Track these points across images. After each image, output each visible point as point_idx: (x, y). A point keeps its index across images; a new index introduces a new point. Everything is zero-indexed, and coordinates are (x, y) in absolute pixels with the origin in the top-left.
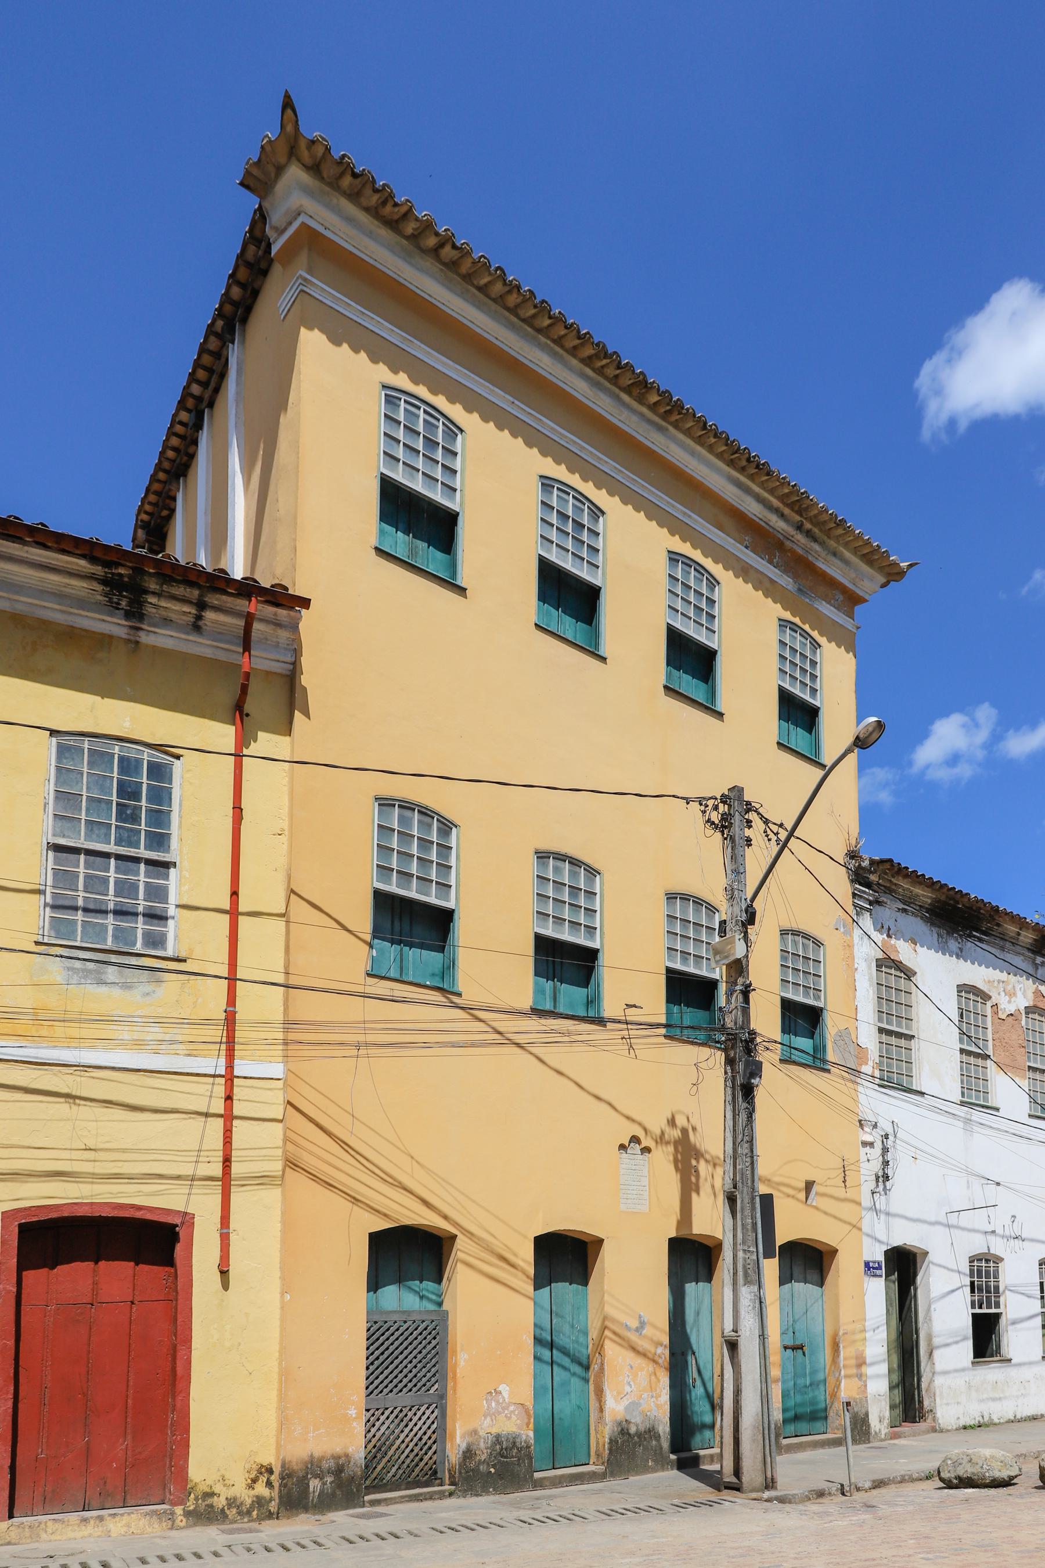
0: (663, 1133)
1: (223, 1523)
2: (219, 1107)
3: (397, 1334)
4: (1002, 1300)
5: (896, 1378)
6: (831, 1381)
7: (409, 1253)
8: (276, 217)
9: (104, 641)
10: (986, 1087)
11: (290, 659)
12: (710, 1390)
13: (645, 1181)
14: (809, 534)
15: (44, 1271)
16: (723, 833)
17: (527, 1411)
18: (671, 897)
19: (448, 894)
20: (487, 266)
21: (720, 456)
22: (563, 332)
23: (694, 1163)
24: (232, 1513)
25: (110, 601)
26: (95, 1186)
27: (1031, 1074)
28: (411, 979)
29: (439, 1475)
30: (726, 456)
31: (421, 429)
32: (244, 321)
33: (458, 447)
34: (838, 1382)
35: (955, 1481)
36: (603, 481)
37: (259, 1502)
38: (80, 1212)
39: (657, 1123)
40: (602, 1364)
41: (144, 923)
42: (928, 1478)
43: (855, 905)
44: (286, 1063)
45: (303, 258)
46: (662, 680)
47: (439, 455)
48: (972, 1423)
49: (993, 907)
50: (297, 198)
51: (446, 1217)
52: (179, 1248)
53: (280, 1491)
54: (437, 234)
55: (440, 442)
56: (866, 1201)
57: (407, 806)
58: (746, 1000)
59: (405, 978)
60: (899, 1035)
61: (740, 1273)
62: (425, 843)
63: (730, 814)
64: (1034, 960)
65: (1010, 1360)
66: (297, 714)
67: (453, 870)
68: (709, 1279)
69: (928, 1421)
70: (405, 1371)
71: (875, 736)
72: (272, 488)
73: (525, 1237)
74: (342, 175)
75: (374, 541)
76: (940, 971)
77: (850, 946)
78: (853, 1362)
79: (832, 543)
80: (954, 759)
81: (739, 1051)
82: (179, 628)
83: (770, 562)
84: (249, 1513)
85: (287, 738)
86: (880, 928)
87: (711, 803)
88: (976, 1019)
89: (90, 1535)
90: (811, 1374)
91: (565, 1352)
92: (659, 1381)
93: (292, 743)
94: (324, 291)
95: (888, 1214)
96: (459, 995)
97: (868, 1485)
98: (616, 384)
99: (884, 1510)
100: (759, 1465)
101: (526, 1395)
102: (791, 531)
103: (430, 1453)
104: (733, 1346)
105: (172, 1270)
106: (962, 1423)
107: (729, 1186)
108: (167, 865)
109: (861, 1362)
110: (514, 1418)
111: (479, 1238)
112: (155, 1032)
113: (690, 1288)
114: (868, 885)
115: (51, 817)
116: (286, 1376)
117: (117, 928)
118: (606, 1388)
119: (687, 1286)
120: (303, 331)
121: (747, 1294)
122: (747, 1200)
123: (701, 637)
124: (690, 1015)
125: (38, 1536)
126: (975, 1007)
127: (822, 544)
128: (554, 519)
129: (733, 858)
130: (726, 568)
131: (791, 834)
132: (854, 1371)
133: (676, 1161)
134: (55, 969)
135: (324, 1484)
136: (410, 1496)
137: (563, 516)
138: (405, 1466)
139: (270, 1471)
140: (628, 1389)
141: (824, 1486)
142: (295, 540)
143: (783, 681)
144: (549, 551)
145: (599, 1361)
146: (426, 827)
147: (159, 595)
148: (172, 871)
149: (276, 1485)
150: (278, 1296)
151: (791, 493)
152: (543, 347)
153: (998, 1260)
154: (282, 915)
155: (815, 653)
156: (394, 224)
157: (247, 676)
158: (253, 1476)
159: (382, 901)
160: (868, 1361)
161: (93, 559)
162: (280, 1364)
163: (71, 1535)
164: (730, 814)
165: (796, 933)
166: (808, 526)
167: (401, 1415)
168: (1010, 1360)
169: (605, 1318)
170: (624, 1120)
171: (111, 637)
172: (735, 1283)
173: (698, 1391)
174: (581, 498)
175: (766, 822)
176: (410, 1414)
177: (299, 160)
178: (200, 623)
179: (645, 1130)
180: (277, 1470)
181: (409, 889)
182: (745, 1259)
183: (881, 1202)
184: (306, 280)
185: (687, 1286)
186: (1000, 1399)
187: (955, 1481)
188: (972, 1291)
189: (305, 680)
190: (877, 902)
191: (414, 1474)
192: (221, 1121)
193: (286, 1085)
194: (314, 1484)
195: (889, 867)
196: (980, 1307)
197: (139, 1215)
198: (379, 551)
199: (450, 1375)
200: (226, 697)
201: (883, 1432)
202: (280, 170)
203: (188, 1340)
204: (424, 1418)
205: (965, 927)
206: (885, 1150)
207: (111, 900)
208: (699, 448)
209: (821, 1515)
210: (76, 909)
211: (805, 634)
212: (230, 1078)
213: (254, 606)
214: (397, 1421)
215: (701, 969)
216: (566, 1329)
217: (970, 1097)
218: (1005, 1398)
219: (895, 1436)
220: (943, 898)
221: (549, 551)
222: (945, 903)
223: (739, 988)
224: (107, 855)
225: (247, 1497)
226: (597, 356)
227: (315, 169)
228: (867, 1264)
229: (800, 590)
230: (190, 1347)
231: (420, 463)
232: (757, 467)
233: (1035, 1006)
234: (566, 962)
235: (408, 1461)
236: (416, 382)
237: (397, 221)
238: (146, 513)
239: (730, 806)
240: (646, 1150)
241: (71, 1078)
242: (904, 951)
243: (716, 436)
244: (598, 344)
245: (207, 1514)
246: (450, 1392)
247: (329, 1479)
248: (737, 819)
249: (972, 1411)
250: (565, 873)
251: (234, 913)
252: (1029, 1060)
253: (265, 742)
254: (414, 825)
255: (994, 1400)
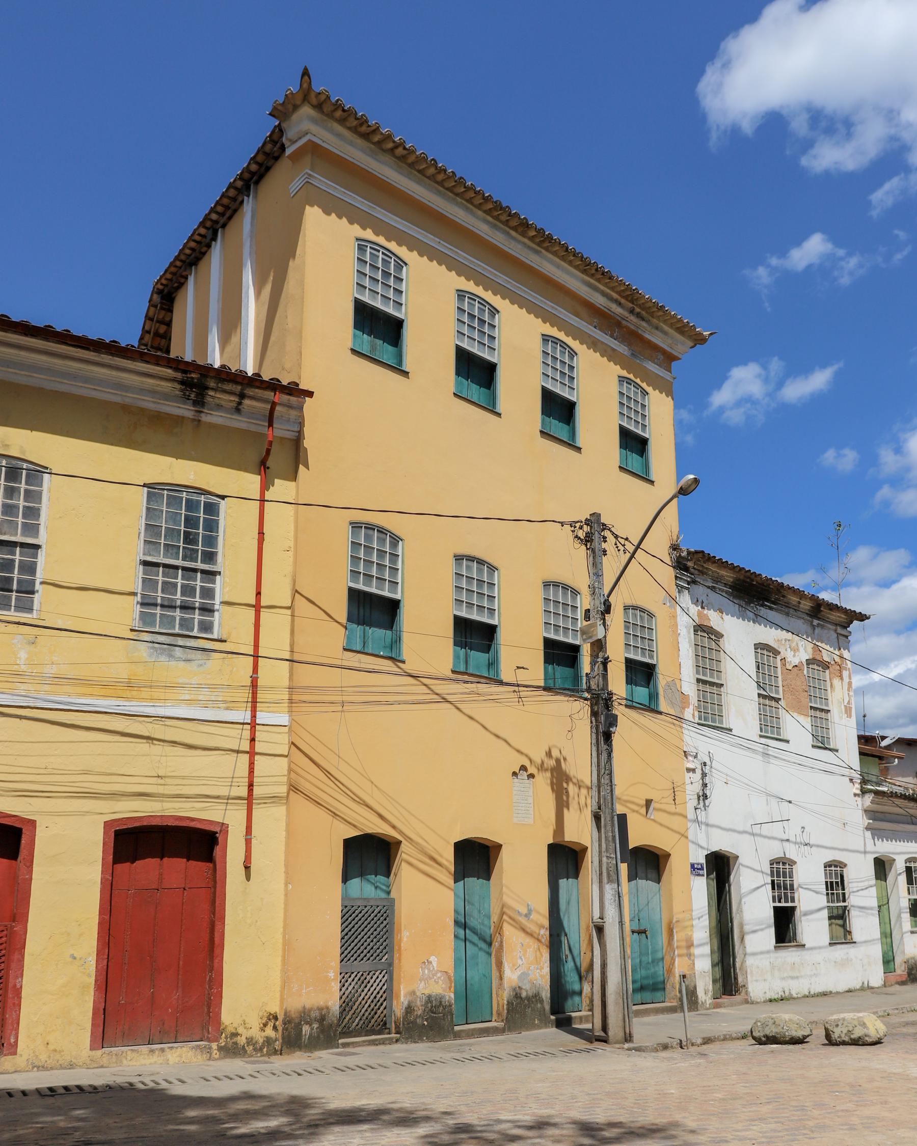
0: (543, 763)
1: (244, 1056)
2: (246, 746)
3: (360, 916)
4: (796, 896)
5: (717, 957)
6: (667, 959)
7: (370, 854)
9: (179, 420)
10: (778, 723)
11: (296, 429)
12: (578, 964)
13: (531, 800)
14: (638, 315)
15: (128, 864)
16: (586, 545)
17: (449, 978)
18: (547, 585)
19: (396, 588)
20: (425, 159)
22: (473, 195)
23: (565, 785)
25: (184, 394)
26: (164, 804)
27: (813, 713)
28: (370, 651)
29: (388, 1026)
30: (581, 267)
31: (380, 265)
32: (257, 183)
33: (404, 276)
34: (673, 960)
35: (764, 1039)
36: (498, 289)
37: (268, 1041)
38: (154, 822)
39: (538, 756)
40: (502, 942)
41: (200, 615)
42: (744, 1037)
43: (677, 585)
44: (290, 712)
45: (308, 159)
47: (391, 282)
48: (776, 997)
49: (779, 584)
51: (394, 827)
53: (283, 1033)
54: (394, 142)
55: (390, 272)
57: (370, 527)
58: (605, 669)
59: (366, 651)
60: (712, 684)
62: (381, 553)
63: (592, 533)
64: (812, 622)
65: (804, 945)
67: (400, 571)
68: (576, 875)
69: (743, 994)
70: (366, 944)
71: (693, 487)
73: (448, 842)
74: (335, 110)
75: (350, 344)
76: (740, 634)
77: (674, 617)
78: (684, 944)
79: (655, 321)
81: (600, 707)
82: (227, 410)
83: (612, 336)
84: (261, 1049)
85: (294, 483)
86: (696, 602)
87: (578, 525)
88: (769, 670)
89: (155, 1062)
90: (652, 953)
91: (474, 931)
92: (542, 956)
94: (321, 182)
95: (707, 825)
96: (404, 662)
97: (699, 1041)
98: (507, 225)
101: (448, 963)
102: (626, 314)
103: (382, 1008)
104: (600, 930)
105: (211, 865)
106: (768, 997)
107: (595, 807)
108: (214, 574)
109: (690, 945)
110: (441, 982)
111: (417, 843)
113: (563, 883)
114: (686, 569)
115: (142, 542)
116: (287, 945)
117: (182, 619)
118: (504, 961)
119: (561, 881)
120: (307, 207)
121: (609, 889)
122: (608, 819)
123: (565, 393)
124: (561, 671)
125: (121, 1062)
126: (768, 661)
127: (648, 322)
128: (466, 319)
130: (581, 343)
132: (684, 951)
133: (552, 784)
134: (143, 651)
135: (312, 1029)
136: (369, 1041)
137: (471, 316)
138: (364, 1018)
140: (520, 962)
142: (300, 347)
143: (623, 421)
144: (462, 341)
145: (499, 939)
146: (382, 541)
147: (215, 390)
148: (218, 577)
149: (280, 1028)
150: (283, 886)
151: (626, 290)
153: (792, 863)
155: (644, 399)
156: (366, 136)
157: (270, 443)
158: (264, 1021)
159: (355, 596)
160: (695, 943)
161: (176, 369)
162: (284, 937)
163: (143, 1062)
164: (592, 533)
165: (635, 608)
166: (638, 310)
167: (362, 978)
168: (804, 945)
169: (503, 906)
170: (516, 753)
171: (183, 417)
172: (601, 881)
173: (570, 965)
174: (483, 302)
175: (616, 537)
176: (368, 978)
177: (309, 103)
178: (240, 407)
179: (531, 760)
181: (370, 586)
182: (608, 863)
183: (702, 816)
184: (310, 175)
185: (561, 881)
186: (797, 978)
187: (764, 1039)
188: (773, 888)
189: (306, 443)
190: (694, 582)
191: (371, 1025)
193: (291, 730)
194: (306, 1029)
195: (701, 557)
196: (780, 902)
197: (199, 826)
198: (353, 351)
199: (396, 948)
200: (255, 457)
201: (708, 1003)
202: (296, 107)
203: (223, 918)
204: (378, 981)
205: (759, 599)
206: (704, 775)
207: (178, 597)
208: (563, 263)
209: (669, 1059)
210: (156, 605)
211: (637, 386)
212: (253, 725)
214: (359, 983)
215: (568, 637)
216: (475, 914)
217: (766, 732)
218: (801, 977)
220: (742, 577)
221: (462, 341)
222: (744, 581)
223: (599, 660)
225: (260, 1037)
226: (495, 209)
227: (319, 107)
228: (692, 866)
229: (632, 354)
230: (224, 923)
231: (379, 288)
232: (603, 274)
233: (814, 659)
234: (474, 635)
235: (367, 1014)
236: (377, 234)
237: (368, 134)
238: (162, 284)
239: (591, 527)
240: (531, 776)
241: (150, 726)
242: (714, 619)
243: (574, 255)
244: (496, 202)
245: (233, 1050)
246: (396, 961)
247: (315, 1026)
248: (596, 537)
250: (475, 570)
252: (811, 702)
253: (281, 489)
254: (374, 540)
255: (792, 978)
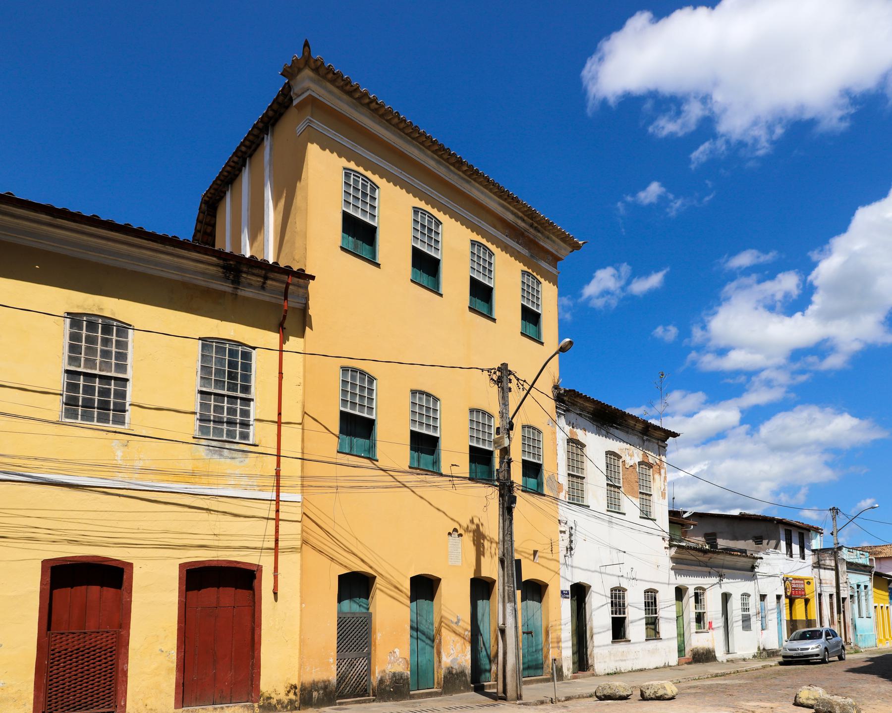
2: (273, 515)
6: (545, 650)
7: (356, 585)
8: (296, 89)
9: (222, 294)
11: (304, 302)
14: (536, 229)
20: (391, 112)
21: (495, 194)
24: (279, 707)
27: (641, 496)
32: (273, 125)
34: (548, 650)
37: (291, 702)
39: (465, 522)
42: (591, 696)
43: (557, 412)
46: (468, 304)
47: (368, 200)
50: (307, 84)
51: (371, 567)
52: (256, 581)
55: (368, 193)
56: (562, 560)
57: (354, 370)
58: (509, 467)
60: (578, 477)
61: (506, 597)
62: (362, 388)
63: (502, 376)
66: (307, 329)
68: (488, 598)
72: (292, 216)
74: (328, 73)
76: (597, 445)
77: (554, 433)
80: (606, 293)
82: (255, 288)
84: (286, 707)
85: (302, 340)
91: (423, 633)
93: (305, 342)
94: (318, 125)
97: (563, 699)
99: (571, 708)
100: (515, 688)
101: (407, 653)
104: (503, 632)
106: (607, 672)
112: (244, 481)
113: (480, 603)
116: (302, 642)
117: (228, 431)
121: (509, 607)
127: (542, 233)
129: (503, 398)
131: (532, 386)
132: (556, 645)
133: (474, 540)
134: (202, 451)
137: (423, 226)
139: (295, 687)
141: (543, 699)
147: (247, 273)
148: (252, 403)
149: (298, 694)
152: (414, 146)
153: (624, 590)
154: (300, 424)
156: (350, 93)
157: (286, 311)
161: (219, 258)
164: (502, 376)
173: (484, 653)
174: (431, 216)
175: (518, 379)
180: (299, 687)
189: (311, 312)
192: (274, 522)
193: (303, 505)
194: (315, 694)
197: (238, 566)
198: (342, 248)
202: (300, 70)
206: (571, 535)
208: (485, 190)
209: (544, 710)
212: (278, 501)
213: (291, 280)
216: (424, 622)
219: (575, 678)
224: (223, 396)
225: (285, 699)
226: (440, 150)
227: (316, 70)
228: (562, 592)
231: (360, 205)
234: (424, 445)
240: (460, 535)
246: (373, 652)
247: (321, 692)
249: (611, 667)
250: (424, 401)
251: (279, 423)
253: (294, 343)
254: (357, 380)
255: (622, 660)
